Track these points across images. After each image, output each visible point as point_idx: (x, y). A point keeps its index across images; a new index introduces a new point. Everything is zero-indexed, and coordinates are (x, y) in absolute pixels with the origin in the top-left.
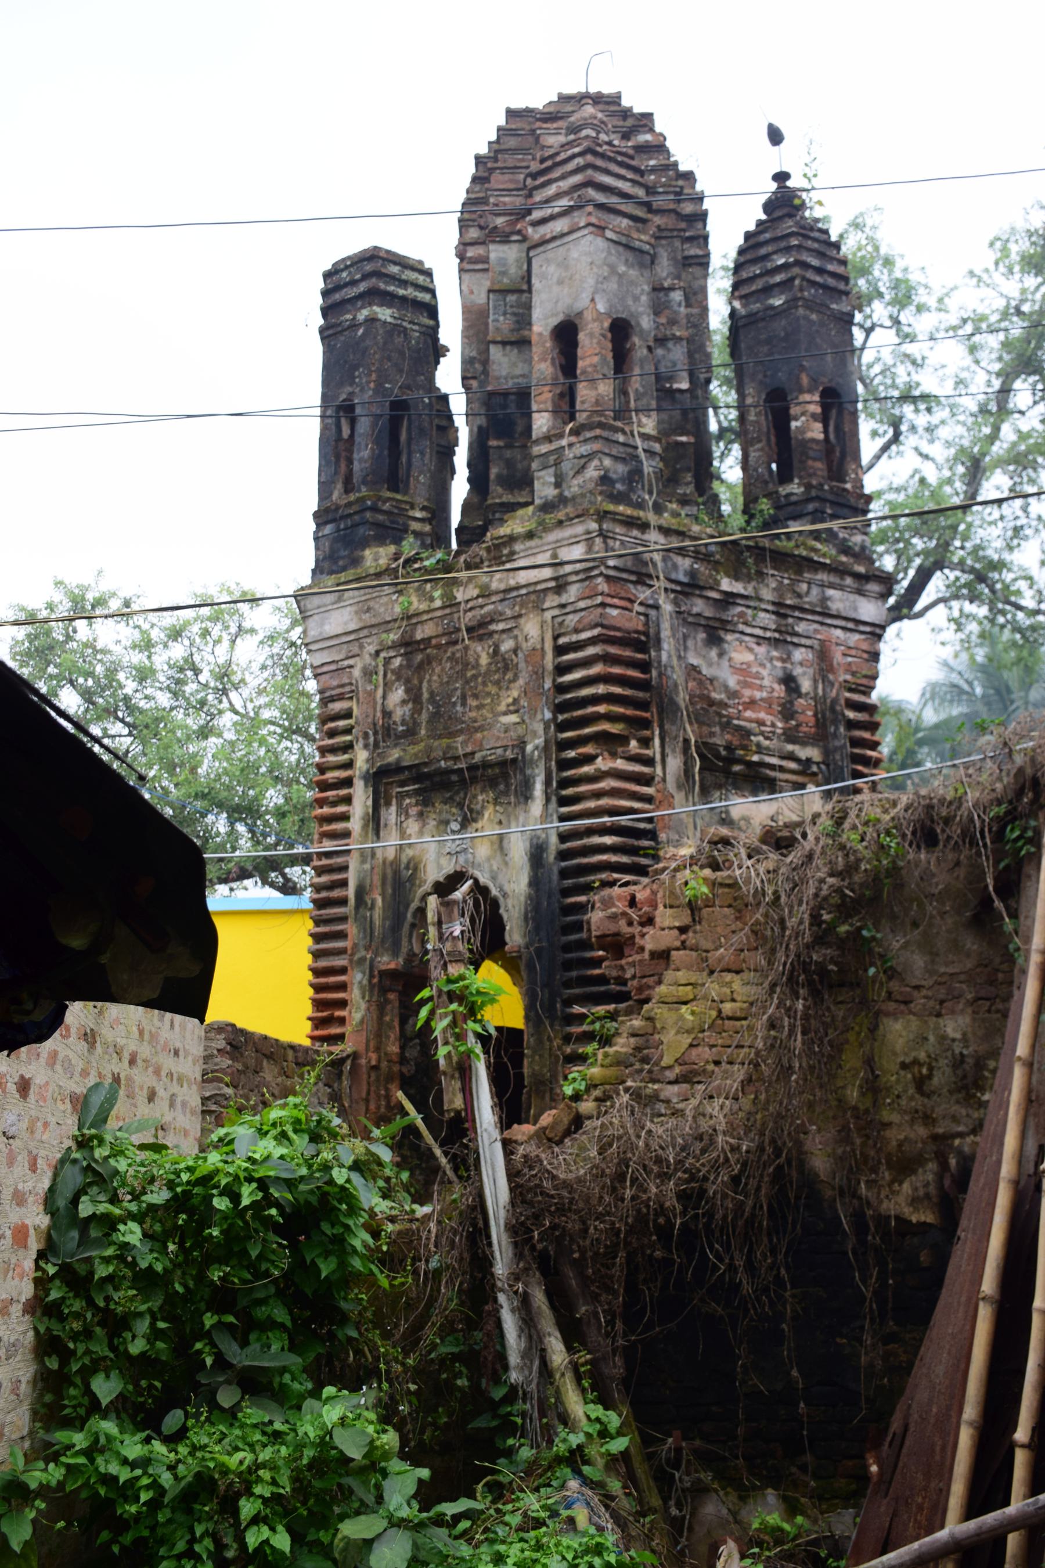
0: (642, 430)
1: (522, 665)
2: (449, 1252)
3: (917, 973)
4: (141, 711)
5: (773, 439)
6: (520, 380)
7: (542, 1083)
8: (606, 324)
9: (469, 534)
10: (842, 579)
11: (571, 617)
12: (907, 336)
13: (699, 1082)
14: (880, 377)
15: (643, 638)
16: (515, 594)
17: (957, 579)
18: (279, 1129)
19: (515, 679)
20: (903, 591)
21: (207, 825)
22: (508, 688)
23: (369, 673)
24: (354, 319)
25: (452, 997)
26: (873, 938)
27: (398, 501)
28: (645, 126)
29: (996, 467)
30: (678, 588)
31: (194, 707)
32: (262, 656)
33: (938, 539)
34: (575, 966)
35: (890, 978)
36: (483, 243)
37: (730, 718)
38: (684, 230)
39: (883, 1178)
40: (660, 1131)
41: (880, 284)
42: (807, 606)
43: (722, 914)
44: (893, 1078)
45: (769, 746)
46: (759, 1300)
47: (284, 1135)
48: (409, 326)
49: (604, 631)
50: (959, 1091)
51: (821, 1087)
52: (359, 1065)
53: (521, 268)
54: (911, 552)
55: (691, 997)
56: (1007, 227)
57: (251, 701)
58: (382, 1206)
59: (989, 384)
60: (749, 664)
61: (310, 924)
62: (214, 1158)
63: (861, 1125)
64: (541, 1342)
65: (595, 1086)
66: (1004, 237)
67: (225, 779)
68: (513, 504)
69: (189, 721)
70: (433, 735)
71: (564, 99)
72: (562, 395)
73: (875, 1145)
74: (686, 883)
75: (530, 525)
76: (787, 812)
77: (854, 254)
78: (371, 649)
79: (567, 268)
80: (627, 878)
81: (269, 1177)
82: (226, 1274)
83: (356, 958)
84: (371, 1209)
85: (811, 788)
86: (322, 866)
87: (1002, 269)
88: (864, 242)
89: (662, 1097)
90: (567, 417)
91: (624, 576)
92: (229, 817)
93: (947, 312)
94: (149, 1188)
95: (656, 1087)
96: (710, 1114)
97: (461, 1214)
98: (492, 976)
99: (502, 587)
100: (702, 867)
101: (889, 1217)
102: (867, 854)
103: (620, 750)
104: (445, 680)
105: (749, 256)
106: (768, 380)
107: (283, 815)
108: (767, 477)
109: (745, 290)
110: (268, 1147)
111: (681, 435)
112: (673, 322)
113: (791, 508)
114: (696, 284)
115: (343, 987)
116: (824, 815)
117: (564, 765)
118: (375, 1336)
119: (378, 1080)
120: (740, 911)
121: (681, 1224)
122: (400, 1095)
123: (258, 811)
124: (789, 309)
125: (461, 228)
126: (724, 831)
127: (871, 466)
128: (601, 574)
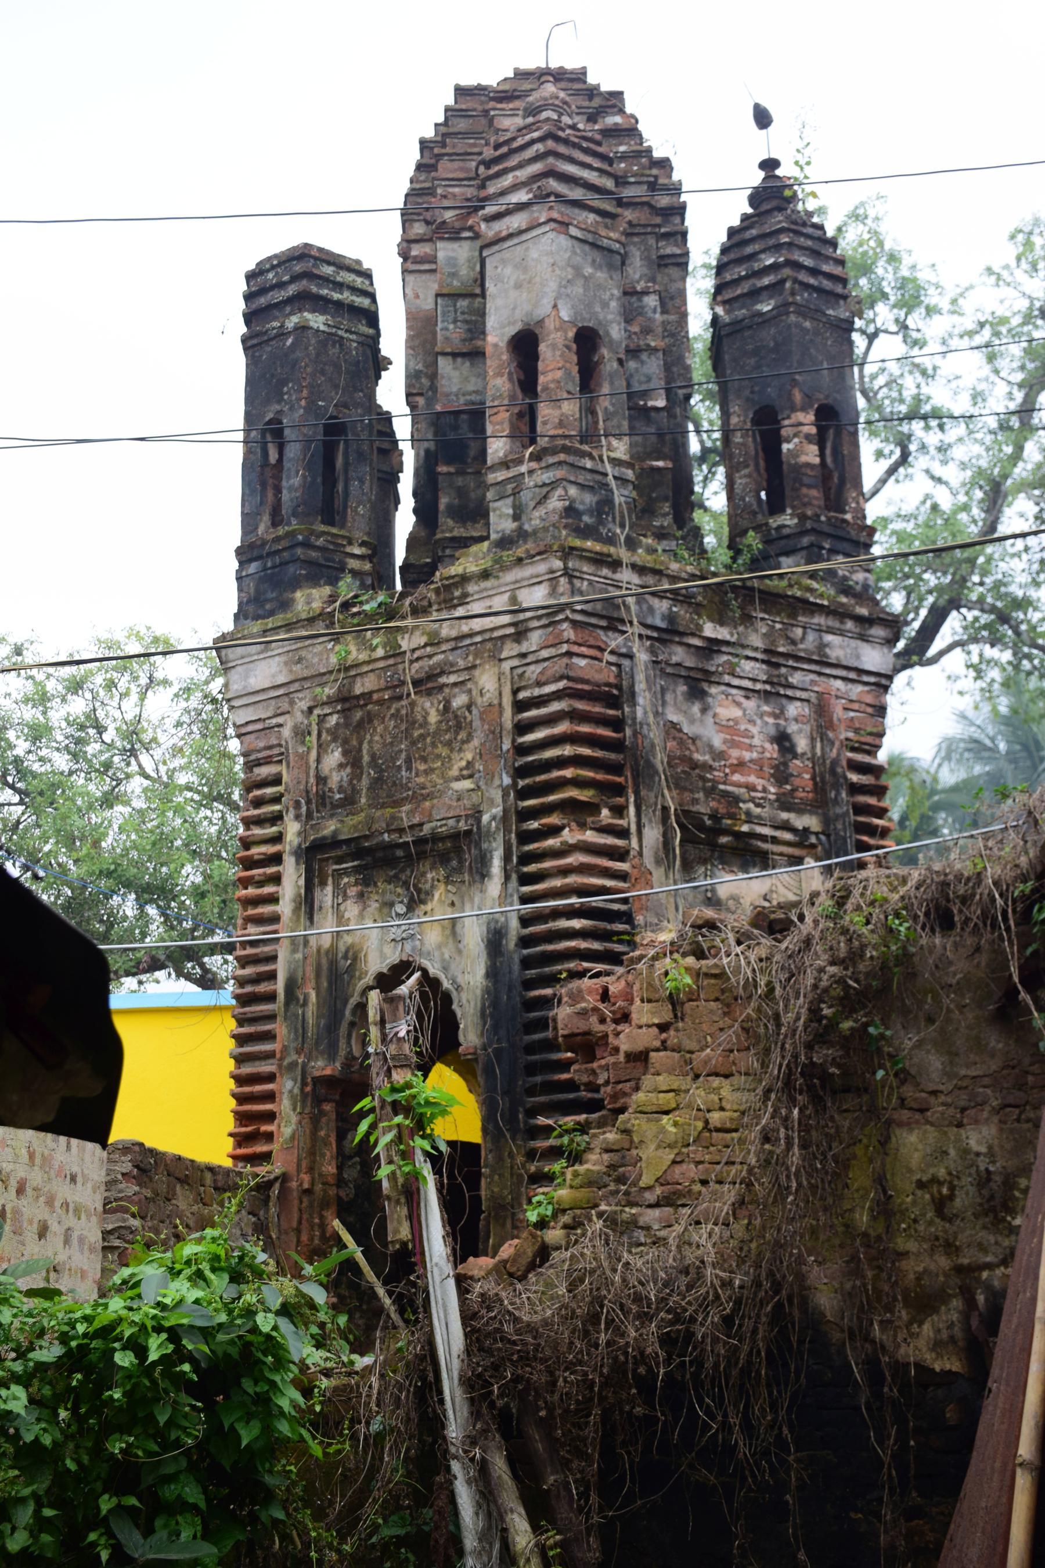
0: (613, 455)
1: (477, 723)
2: (393, 1412)
3: (935, 1076)
4: (35, 775)
5: (762, 463)
6: (473, 397)
7: (503, 1207)
8: (571, 334)
9: (417, 573)
10: (842, 623)
11: (532, 668)
12: (915, 342)
13: (684, 1205)
14: (885, 390)
15: (615, 692)
16: (468, 642)
17: (976, 619)
18: (194, 1268)
19: (467, 741)
20: (913, 634)
21: (112, 908)
22: (460, 750)
23: (301, 734)
24: (282, 326)
25: (396, 1108)
26: (882, 1036)
27: (334, 535)
28: (614, 106)
29: (1019, 491)
30: (655, 635)
31: (97, 771)
32: (176, 711)
33: (954, 574)
34: (539, 1071)
35: (903, 1082)
36: (430, 240)
37: (715, 782)
38: (659, 226)
39: (900, 1318)
40: (639, 1264)
41: (884, 284)
42: (802, 654)
43: (707, 1009)
44: (909, 1199)
45: (760, 813)
46: (758, 1465)
47: (199, 1274)
48: (346, 335)
49: (571, 684)
50: (986, 1215)
51: (825, 1209)
52: (290, 1190)
53: (473, 269)
54: (923, 589)
55: (674, 1106)
56: (1029, 218)
57: (165, 763)
58: (315, 1357)
59: (1010, 396)
60: (736, 721)
61: (232, 1024)
62: (116, 1304)
63: (872, 1255)
64: (502, 1519)
65: (564, 1211)
66: (1027, 229)
67: (134, 854)
68: (466, 538)
69: (92, 787)
70: (375, 804)
71: (521, 75)
72: (520, 415)
73: (890, 1278)
74: (666, 974)
75: (486, 563)
76: (782, 890)
77: (855, 249)
78: (304, 705)
79: (525, 270)
80: (599, 967)
81: (182, 1325)
82: (129, 1445)
83: (285, 1063)
84: (302, 1361)
85: (810, 863)
86: (247, 956)
87: (1024, 265)
88: (866, 236)
89: (641, 1224)
90: (526, 440)
91: (593, 620)
92: (137, 899)
93: (963, 315)
94: (38, 1343)
95: (634, 1211)
96: (697, 1242)
97: (407, 1365)
98: (444, 1082)
99: (454, 633)
100: (684, 955)
101: (908, 1364)
102: (874, 939)
103: (590, 820)
104: (389, 740)
105: (732, 256)
106: (756, 397)
107: (203, 895)
108: (755, 507)
109: (728, 294)
110: (181, 1289)
111: (657, 460)
112: (647, 331)
113: (783, 542)
114: (674, 287)
115: (270, 1097)
116: (823, 894)
117: (526, 837)
118: (306, 1516)
119: (311, 1206)
120: (728, 1006)
121: (665, 1373)
122: (337, 1224)
123: (171, 890)
124: (780, 315)
125: (404, 223)
126: (710, 913)
127: (875, 492)
128: (567, 619)
